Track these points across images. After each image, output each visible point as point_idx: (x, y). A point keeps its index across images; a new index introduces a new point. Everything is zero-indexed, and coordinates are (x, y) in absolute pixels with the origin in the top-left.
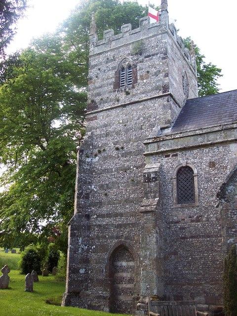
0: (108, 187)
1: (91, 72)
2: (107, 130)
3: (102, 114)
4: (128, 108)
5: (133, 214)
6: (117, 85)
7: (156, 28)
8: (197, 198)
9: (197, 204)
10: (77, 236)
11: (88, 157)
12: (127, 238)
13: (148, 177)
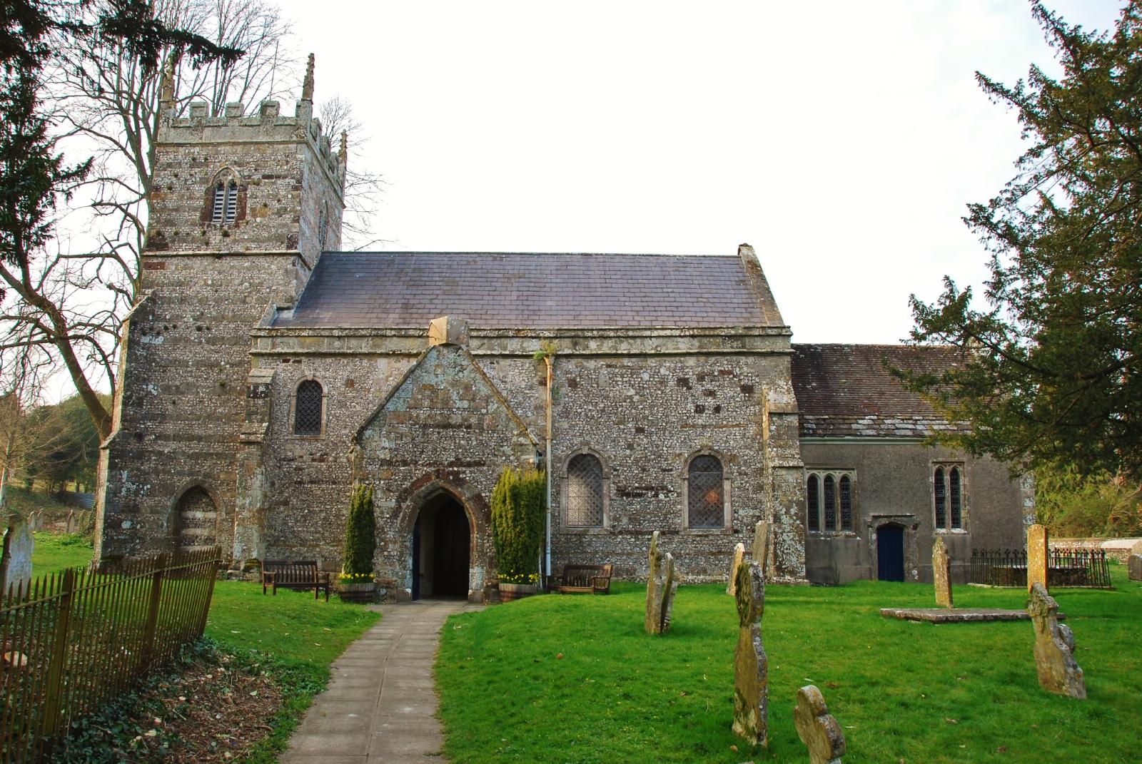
0: (178, 391)
3: (175, 261)
5: (222, 440)
7: (288, 128)
8: (323, 428)
9: (323, 436)
10: (121, 469)
11: (145, 334)
12: (206, 476)
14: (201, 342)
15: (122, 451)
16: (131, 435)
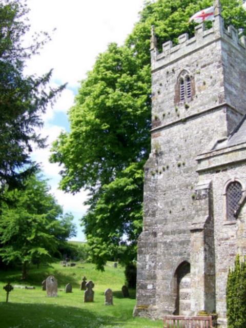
2: (170, 146)
4: (188, 124)
6: (178, 99)
10: (145, 254)
13: (199, 195)
14: (181, 173)
15: (146, 243)
16: (150, 233)
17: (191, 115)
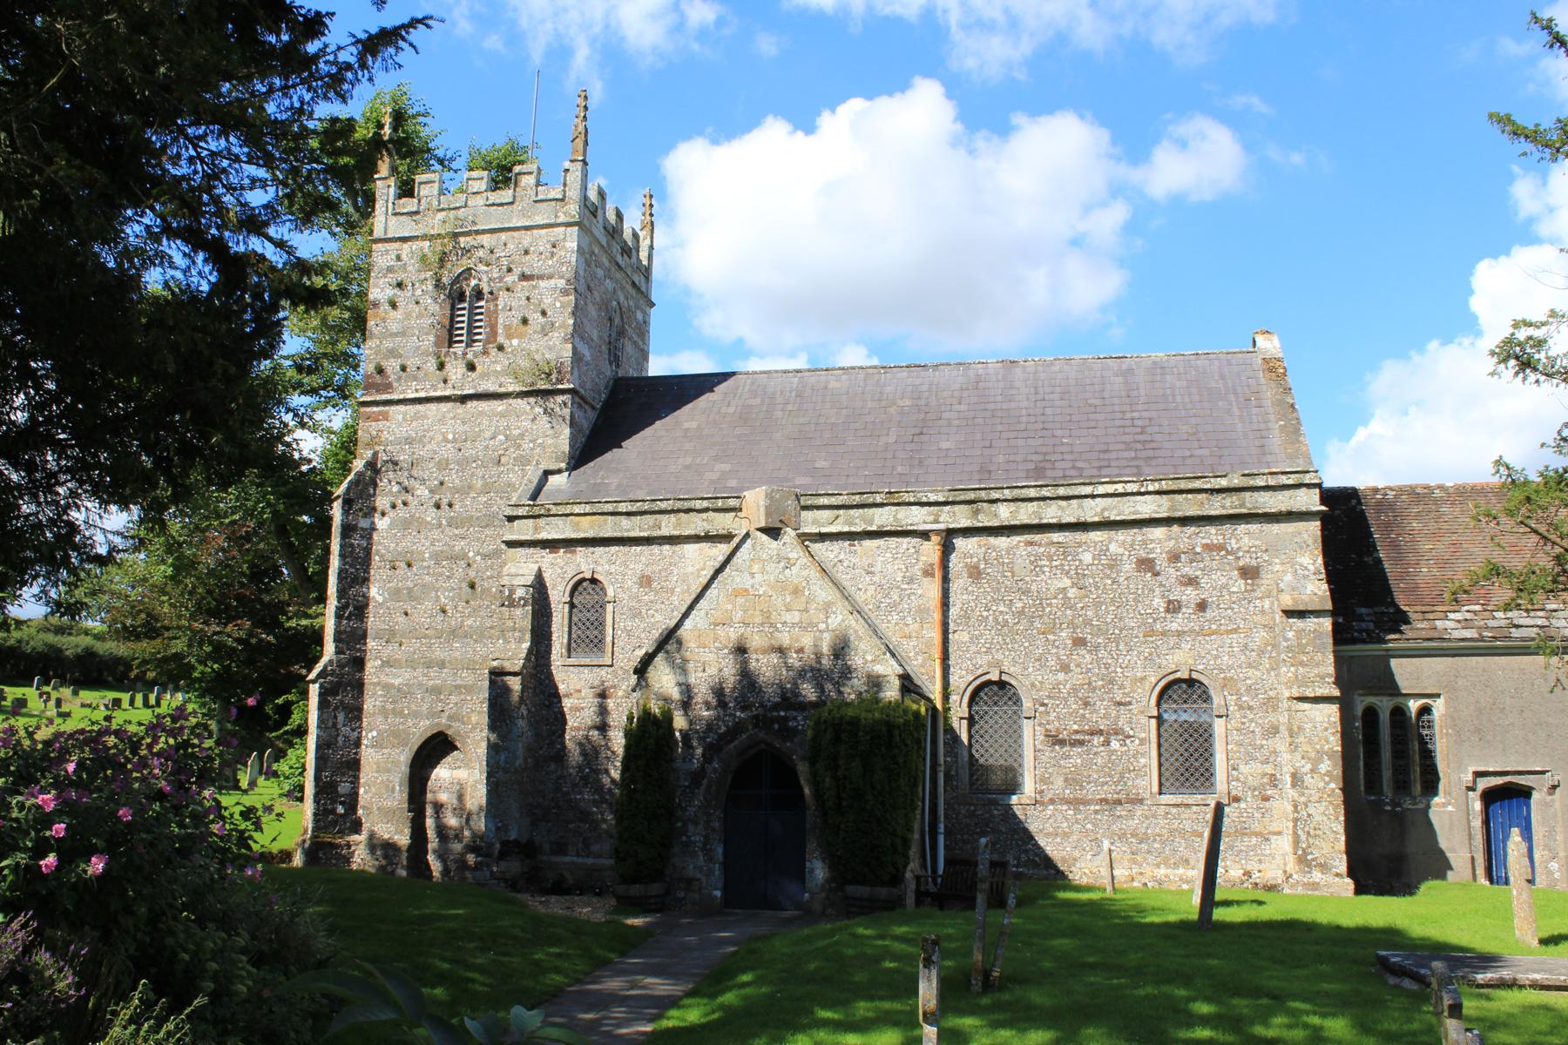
1: (376, 286)
4: (471, 405)
13: (510, 596)
14: (440, 525)
17: (480, 390)
